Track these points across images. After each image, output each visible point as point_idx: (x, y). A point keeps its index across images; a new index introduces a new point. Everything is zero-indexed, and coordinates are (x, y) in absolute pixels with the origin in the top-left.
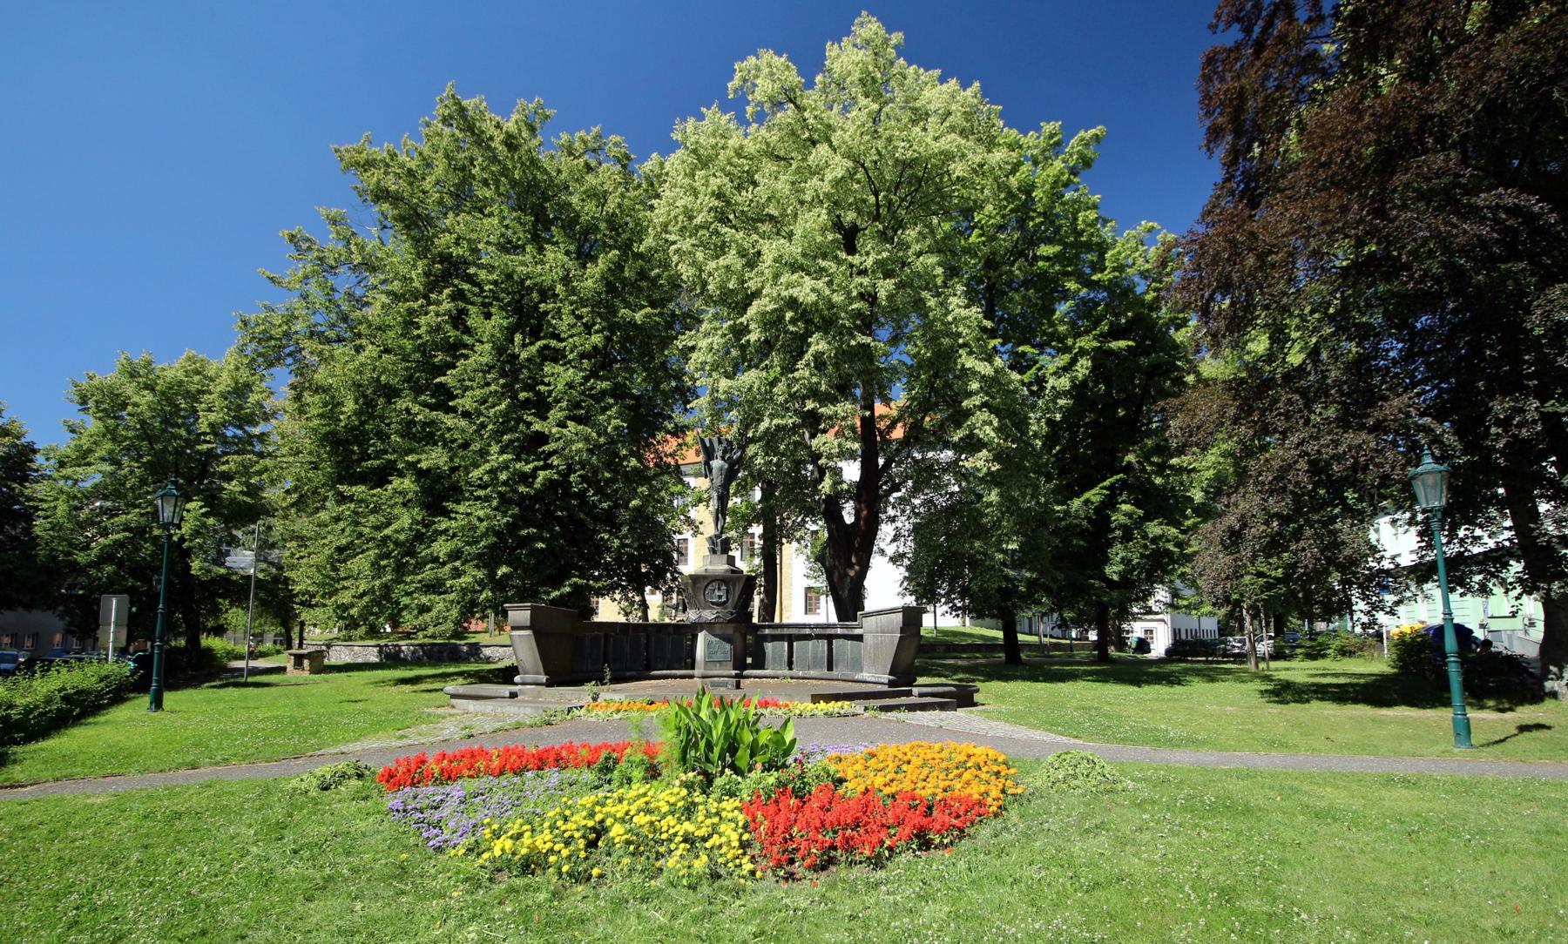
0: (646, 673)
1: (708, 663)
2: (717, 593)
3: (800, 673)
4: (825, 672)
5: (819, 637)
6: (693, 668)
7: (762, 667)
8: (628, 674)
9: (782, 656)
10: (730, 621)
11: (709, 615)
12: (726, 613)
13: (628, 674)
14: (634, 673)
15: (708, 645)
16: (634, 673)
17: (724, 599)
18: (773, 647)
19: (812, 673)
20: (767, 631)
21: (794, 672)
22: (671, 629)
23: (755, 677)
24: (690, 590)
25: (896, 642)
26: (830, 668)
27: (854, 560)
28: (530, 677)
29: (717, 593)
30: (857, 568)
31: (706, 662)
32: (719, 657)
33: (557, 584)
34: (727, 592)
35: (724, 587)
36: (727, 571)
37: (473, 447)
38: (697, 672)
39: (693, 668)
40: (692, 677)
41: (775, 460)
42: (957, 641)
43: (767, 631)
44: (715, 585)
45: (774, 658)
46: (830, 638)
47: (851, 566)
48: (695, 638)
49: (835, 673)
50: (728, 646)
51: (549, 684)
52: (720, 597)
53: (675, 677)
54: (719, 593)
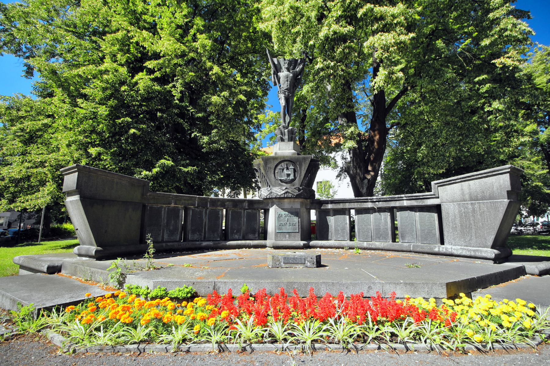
0: (223, 243)
1: (278, 234)
2: (286, 172)
3: (365, 244)
4: (389, 244)
5: (381, 210)
6: (265, 238)
7: (326, 238)
8: (205, 244)
9: (344, 229)
10: (297, 197)
11: (278, 191)
12: (293, 190)
13: (205, 244)
14: (211, 243)
15: (279, 217)
16: (211, 243)
17: (292, 177)
18: (336, 221)
19: (378, 244)
20: (330, 206)
21: (447, 247)
22: (246, 205)
23: (321, 247)
24: (262, 171)
25: (506, 206)
26: (352, 237)
27: (370, 168)
28: (84, 248)
29: (286, 172)
30: (372, 173)
31: (277, 234)
32: (288, 228)
33: (149, 166)
34: (295, 171)
35: (292, 167)
36: (294, 154)
37: (50, 27)
38: (268, 242)
39: (265, 238)
40: (264, 246)
41: (332, 64)
42: (192, 251)
43: (330, 206)
44: (284, 165)
45: (336, 230)
46: (391, 210)
47: (368, 172)
48: (266, 212)
49: (399, 244)
50: (296, 219)
51: (100, 256)
52: (288, 175)
53: (249, 247)
54: (287, 172)
